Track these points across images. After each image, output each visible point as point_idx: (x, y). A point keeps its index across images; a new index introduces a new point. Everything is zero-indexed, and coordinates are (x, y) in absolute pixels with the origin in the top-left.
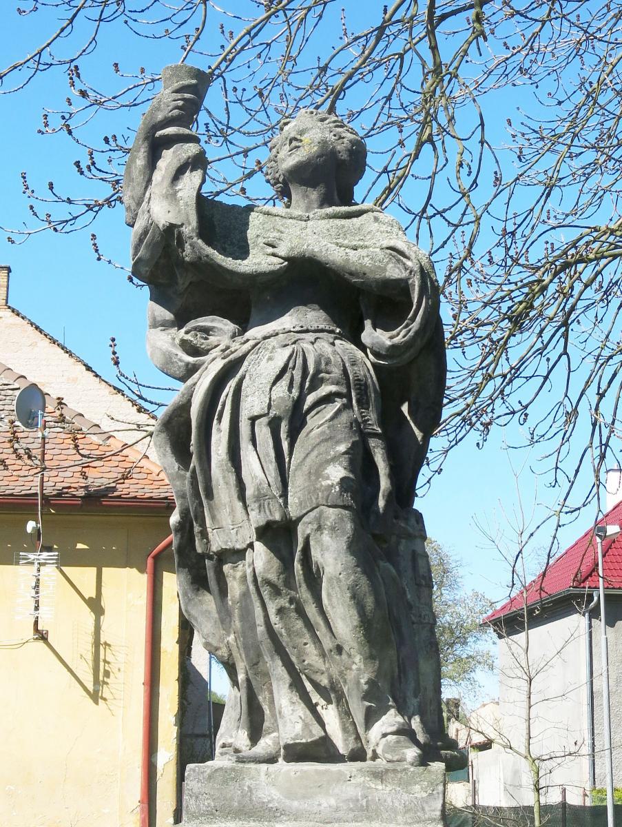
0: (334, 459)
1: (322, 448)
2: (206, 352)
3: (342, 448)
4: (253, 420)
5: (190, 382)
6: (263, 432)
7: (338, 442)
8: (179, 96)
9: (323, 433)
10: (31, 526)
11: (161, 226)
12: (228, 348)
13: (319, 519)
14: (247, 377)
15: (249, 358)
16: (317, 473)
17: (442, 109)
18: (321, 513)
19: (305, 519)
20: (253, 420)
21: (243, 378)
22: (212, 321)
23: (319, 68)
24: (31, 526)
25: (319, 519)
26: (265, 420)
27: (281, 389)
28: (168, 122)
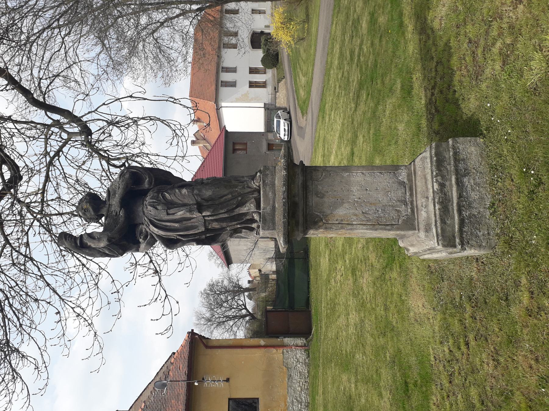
0: (180, 192)
1: (177, 195)
2: (147, 232)
3: (177, 191)
4: (168, 214)
5: (156, 237)
6: (171, 211)
7: (175, 192)
8: (67, 239)
9: (173, 196)
10: (196, 384)
11: (108, 243)
12: (146, 225)
13: (197, 195)
14: (155, 218)
15: (150, 218)
16: (184, 196)
17: (159, 53)
18: (195, 194)
19: (197, 198)
20: (168, 214)
21: (155, 219)
22: (138, 231)
23: (39, 226)
24: (196, 384)
25: (197, 195)
26: (168, 211)
27: (159, 207)
28: (76, 243)
